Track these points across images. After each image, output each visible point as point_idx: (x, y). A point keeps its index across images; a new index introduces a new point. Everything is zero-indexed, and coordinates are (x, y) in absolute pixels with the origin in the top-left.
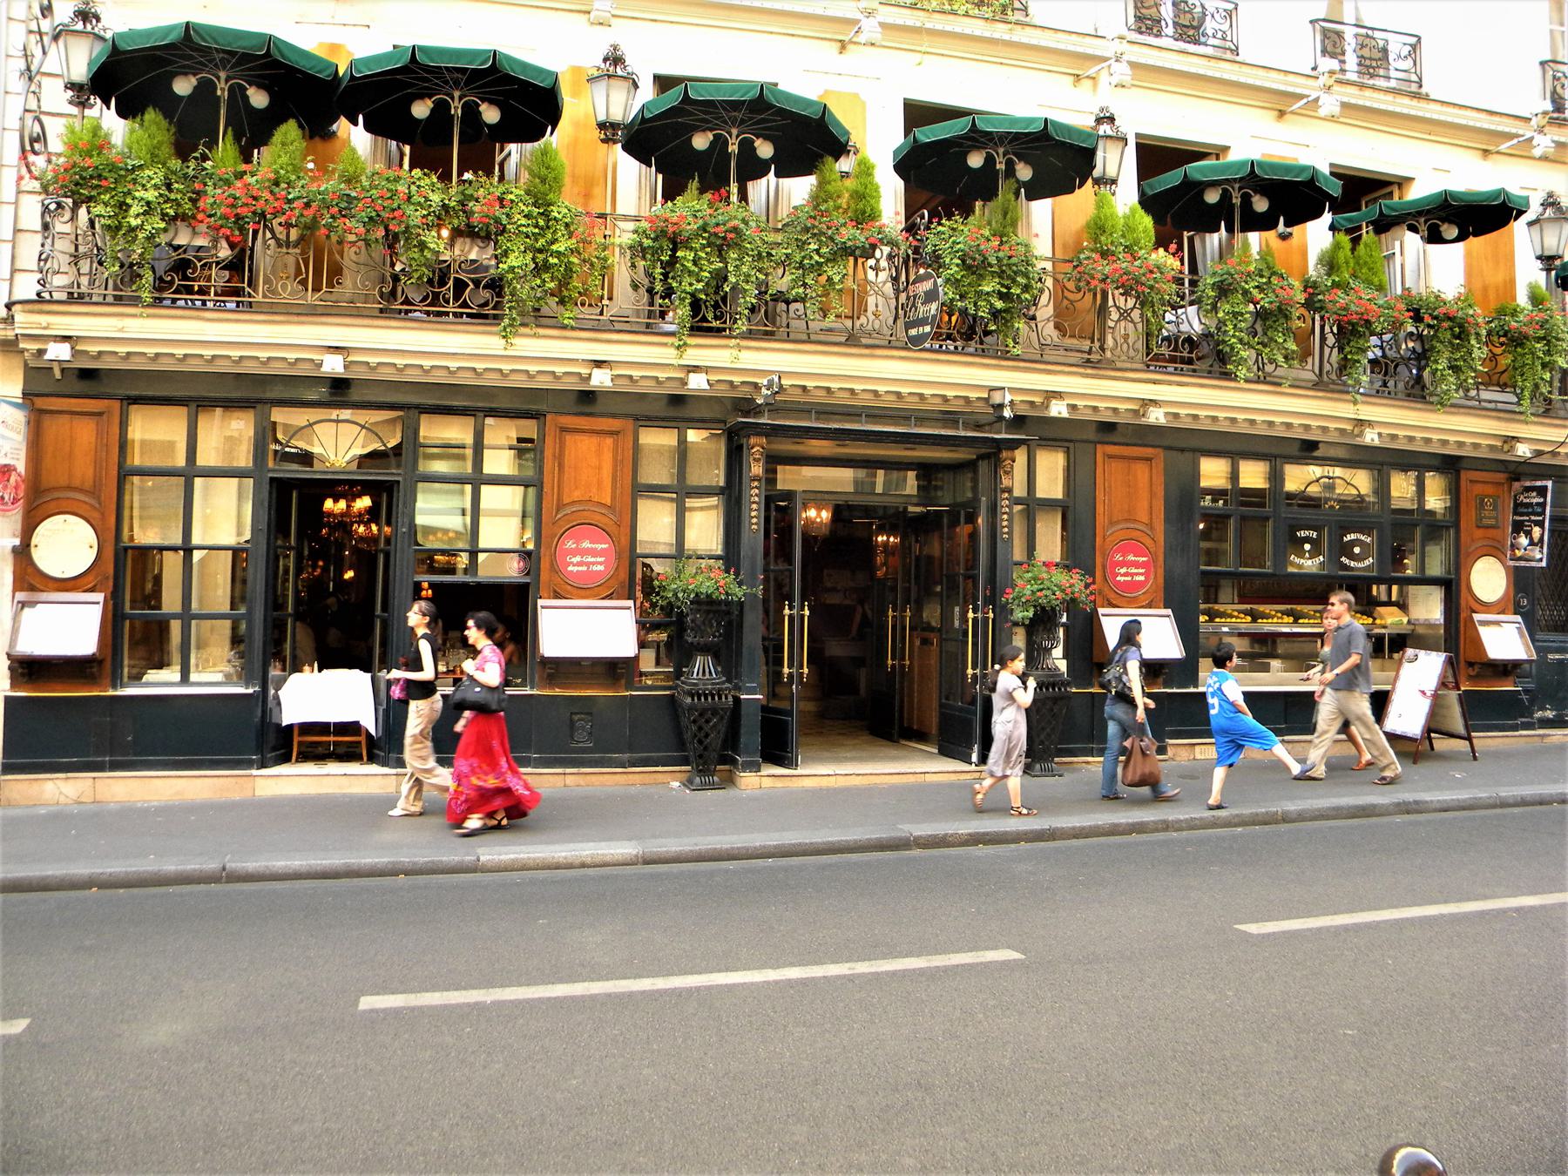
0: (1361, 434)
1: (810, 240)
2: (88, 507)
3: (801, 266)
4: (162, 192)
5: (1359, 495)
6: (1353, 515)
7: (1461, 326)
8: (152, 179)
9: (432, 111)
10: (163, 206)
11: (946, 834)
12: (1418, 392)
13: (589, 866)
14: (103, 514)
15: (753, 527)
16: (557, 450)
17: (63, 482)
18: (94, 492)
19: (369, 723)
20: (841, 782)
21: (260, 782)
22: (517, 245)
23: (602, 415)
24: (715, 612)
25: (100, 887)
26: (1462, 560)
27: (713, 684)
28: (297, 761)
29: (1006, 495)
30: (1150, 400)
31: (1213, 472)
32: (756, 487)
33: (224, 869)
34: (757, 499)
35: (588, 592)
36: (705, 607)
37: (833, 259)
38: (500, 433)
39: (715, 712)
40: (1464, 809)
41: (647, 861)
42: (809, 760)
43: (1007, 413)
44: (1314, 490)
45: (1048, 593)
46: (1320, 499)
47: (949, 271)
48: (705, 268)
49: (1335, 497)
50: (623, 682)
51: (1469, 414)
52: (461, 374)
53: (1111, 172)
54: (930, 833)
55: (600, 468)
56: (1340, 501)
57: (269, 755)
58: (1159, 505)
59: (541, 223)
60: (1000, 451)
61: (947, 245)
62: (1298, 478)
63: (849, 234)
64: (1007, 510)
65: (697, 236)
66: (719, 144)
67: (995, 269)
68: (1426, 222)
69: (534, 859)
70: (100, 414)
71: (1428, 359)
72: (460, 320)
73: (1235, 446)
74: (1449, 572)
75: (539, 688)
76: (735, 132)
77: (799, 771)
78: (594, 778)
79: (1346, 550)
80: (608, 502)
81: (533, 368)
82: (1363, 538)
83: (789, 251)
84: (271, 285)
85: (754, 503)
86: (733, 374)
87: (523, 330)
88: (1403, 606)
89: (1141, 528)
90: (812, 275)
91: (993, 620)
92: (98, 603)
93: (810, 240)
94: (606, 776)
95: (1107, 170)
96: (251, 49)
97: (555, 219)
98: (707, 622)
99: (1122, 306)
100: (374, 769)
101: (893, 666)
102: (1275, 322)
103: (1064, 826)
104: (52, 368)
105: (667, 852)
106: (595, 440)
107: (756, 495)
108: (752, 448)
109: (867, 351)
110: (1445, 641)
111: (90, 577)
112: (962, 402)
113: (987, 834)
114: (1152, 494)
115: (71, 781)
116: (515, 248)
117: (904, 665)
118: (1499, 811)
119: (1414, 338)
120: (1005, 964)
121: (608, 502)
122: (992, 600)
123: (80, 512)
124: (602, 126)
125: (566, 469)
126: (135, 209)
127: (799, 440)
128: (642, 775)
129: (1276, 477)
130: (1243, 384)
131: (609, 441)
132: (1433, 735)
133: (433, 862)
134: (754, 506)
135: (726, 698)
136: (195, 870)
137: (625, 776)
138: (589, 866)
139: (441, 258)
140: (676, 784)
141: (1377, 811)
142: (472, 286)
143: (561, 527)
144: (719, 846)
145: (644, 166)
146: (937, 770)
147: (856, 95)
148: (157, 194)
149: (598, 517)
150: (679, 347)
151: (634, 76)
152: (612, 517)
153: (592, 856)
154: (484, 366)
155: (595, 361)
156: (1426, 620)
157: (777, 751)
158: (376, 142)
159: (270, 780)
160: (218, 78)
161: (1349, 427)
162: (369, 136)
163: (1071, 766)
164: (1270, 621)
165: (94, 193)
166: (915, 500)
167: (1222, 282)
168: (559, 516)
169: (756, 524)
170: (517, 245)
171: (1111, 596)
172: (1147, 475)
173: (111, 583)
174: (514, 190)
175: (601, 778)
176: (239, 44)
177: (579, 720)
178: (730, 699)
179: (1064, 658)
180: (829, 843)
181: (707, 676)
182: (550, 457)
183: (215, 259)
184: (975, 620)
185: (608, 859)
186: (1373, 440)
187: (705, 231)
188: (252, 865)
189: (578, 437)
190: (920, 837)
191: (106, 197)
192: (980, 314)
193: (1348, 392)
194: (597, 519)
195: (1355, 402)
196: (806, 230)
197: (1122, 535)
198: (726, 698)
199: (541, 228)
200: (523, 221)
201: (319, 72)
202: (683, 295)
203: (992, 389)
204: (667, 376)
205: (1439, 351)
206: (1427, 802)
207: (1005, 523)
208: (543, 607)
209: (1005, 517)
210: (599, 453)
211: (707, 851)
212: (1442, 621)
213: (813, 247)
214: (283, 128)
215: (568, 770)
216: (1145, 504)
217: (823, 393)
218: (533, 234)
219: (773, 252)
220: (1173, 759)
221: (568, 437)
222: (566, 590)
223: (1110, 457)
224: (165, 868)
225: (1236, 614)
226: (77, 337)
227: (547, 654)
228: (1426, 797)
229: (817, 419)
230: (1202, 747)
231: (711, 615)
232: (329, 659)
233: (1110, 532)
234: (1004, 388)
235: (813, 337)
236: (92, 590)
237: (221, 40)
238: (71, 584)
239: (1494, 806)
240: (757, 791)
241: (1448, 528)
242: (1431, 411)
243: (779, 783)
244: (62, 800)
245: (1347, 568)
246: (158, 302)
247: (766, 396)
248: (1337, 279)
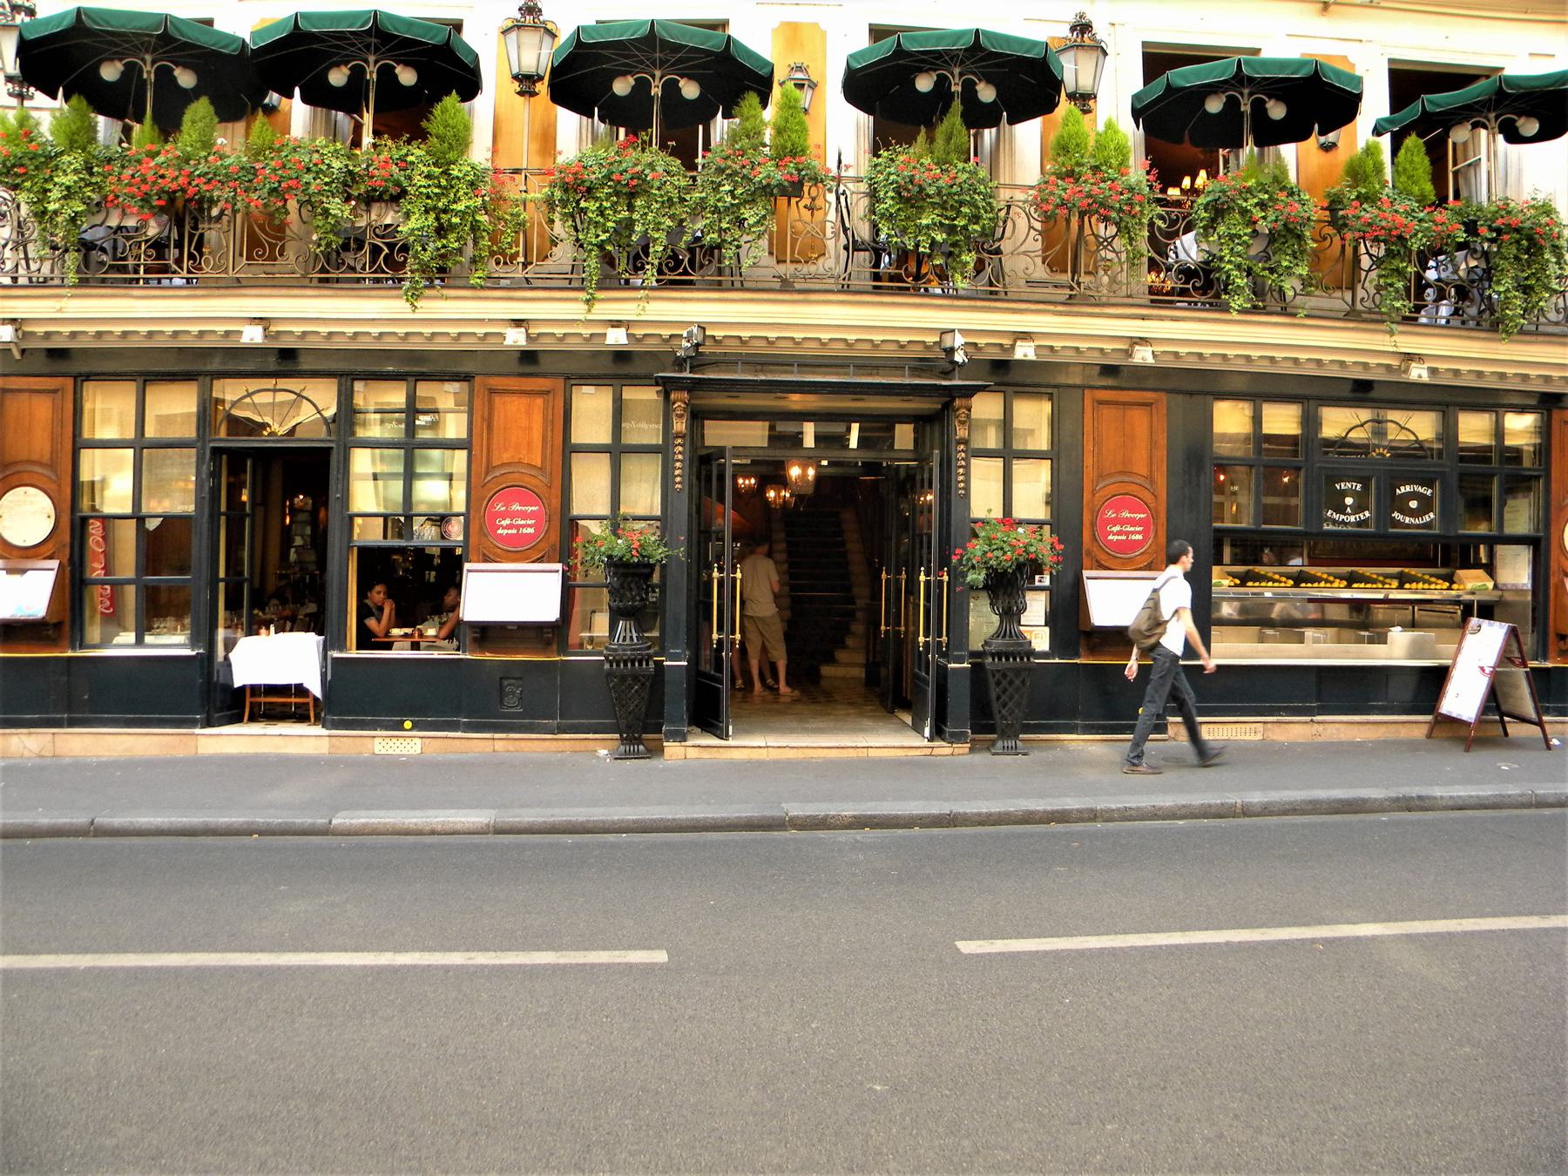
0: (1406, 371)
1: (725, 182)
2: (45, 479)
3: (716, 210)
4: (82, 176)
5: (1417, 441)
6: (1412, 460)
7: (1530, 239)
8: (72, 164)
9: (350, 77)
10: (85, 190)
11: (827, 815)
13: (439, 834)
14: (59, 485)
15: (677, 486)
16: (486, 413)
17: (24, 456)
18: (52, 465)
19: (316, 689)
20: (775, 755)
21: (202, 740)
22: (417, 209)
23: (544, 375)
24: (634, 575)
25: (261, 833)
26: (1553, 515)
27: (634, 650)
29: (962, 447)
30: (1140, 338)
32: (962, 451)
33: (92, 823)
34: (680, 457)
35: (519, 555)
36: (621, 570)
37: (751, 201)
38: (445, 396)
39: (636, 678)
40: (1486, 807)
41: (499, 831)
42: (742, 731)
44: (1358, 436)
45: (999, 553)
46: (1366, 446)
47: (883, 206)
48: (610, 217)
49: (1386, 443)
50: (555, 646)
51: (1549, 343)
52: (806, 345)
54: (808, 814)
55: (530, 429)
56: (1391, 449)
57: (217, 715)
58: (1161, 454)
59: (443, 182)
60: (953, 399)
61: (882, 178)
62: (1337, 422)
64: (963, 463)
65: (603, 185)
67: (936, 200)
68: (1497, 118)
69: (385, 824)
70: (55, 391)
71: (1490, 280)
72: (380, 285)
74: (1537, 530)
75: (472, 652)
76: (658, 73)
77: (731, 742)
78: (523, 743)
79: (1401, 504)
80: (539, 464)
82: (1421, 490)
83: (704, 195)
84: (195, 260)
85: (960, 467)
86: (659, 327)
87: (427, 292)
88: (1490, 569)
89: (1138, 481)
90: (727, 219)
91: (741, 580)
92: (52, 570)
93: (725, 182)
94: (457, 742)
95: (1081, 83)
96: (147, 29)
97: (458, 178)
98: (625, 585)
99: (1102, 234)
100: (318, 730)
101: (886, 631)
102: (1284, 243)
103: (968, 811)
104: (10, 350)
105: (519, 822)
106: (525, 400)
107: (680, 453)
108: (674, 404)
109: (801, 297)
110: (1534, 610)
111: (50, 545)
112: (894, 347)
113: (875, 817)
115: (33, 737)
116: (416, 210)
117: (899, 631)
119: (1478, 255)
121: (539, 464)
122: (944, 561)
123: (39, 484)
125: (495, 431)
126: (55, 194)
127: (783, 395)
128: (572, 742)
129: (1310, 422)
130: (1235, 316)
131: (539, 401)
132: (1506, 719)
133: (286, 823)
134: (678, 464)
135: (647, 664)
136: (65, 823)
137: (555, 743)
138: (439, 834)
139: (357, 225)
140: (603, 752)
142: (386, 251)
143: (490, 490)
144: (574, 819)
145: (585, 118)
146: (881, 745)
148: (75, 178)
149: (527, 479)
150: (588, 301)
151: (1103, 44)
152: (543, 479)
153: (443, 823)
154: (749, 334)
155: (513, 320)
156: (1513, 585)
157: (707, 717)
158: (314, 117)
162: (307, 108)
163: (1050, 744)
164: (1316, 585)
165: (18, 181)
166: (911, 456)
167: (1216, 200)
168: (488, 478)
169: (679, 483)
172: (1146, 424)
173: (67, 551)
174: (415, 151)
175: (530, 743)
176: (133, 25)
177: (509, 685)
178: (652, 665)
179: (1046, 625)
181: (628, 642)
182: (479, 419)
183: (144, 238)
185: (459, 827)
186: (1420, 376)
187: (610, 180)
188: (118, 821)
189: (507, 398)
190: (797, 817)
191: (28, 184)
192: (921, 249)
193: (1383, 322)
194: (527, 481)
195: (1391, 333)
196: (720, 171)
197: (1112, 489)
198: (647, 664)
199: (445, 188)
200: (424, 182)
201: (224, 47)
202: (590, 247)
203: (944, 332)
204: (908, 339)
205: (1502, 270)
206: (1435, 798)
207: (961, 478)
208: (469, 571)
209: (961, 471)
210: (529, 413)
211: (635, 822)
212: (1529, 586)
213: (727, 188)
215: (497, 736)
218: (436, 194)
219: (688, 197)
220: (1174, 739)
221: (497, 399)
222: (495, 554)
223: (1101, 403)
224: (39, 821)
225: (1277, 577)
226: (22, 319)
227: (1096, 624)
228: (1438, 792)
229: (911, 376)
230: (1211, 726)
231: (630, 579)
232: (289, 623)
233: (1101, 485)
234: (953, 331)
236: (50, 557)
237: (113, 23)
238: (31, 552)
239: (1529, 805)
240: (680, 762)
241: (1537, 478)
243: (706, 754)
244: (26, 753)
246: (83, 283)
247: (687, 349)
248: (1363, 191)
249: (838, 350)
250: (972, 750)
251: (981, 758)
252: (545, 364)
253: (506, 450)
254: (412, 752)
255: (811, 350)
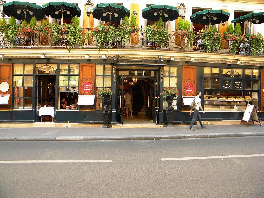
3: (121, 35)
6: (238, 78)
7: (258, 40)
12: (251, 54)
17: (4, 77)
18: (9, 78)
22: (70, 35)
26: (261, 87)
28: (42, 121)
31: (207, 71)
38: (75, 67)
43: (161, 60)
44: (229, 73)
46: (230, 75)
53: (183, 14)
56: (234, 76)
58: (196, 77)
63: (129, 29)
66: (108, 15)
68: (252, 20)
70: (9, 66)
73: (212, 65)
74: (259, 89)
75: (79, 110)
77: (123, 125)
81: (134, 56)
100: (54, 123)
106: (88, 67)
109: (135, 50)
114: (194, 75)
118: (258, 137)
120: (109, 163)
122: (159, 94)
124: (87, 13)
126: (9, 33)
129: (221, 71)
130: (208, 53)
131: (91, 67)
140: (101, 127)
141: (230, 136)
147: (137, 4)
150: (99, 51)
157: (119, 120)
159: (36, 124)
160: (24, 10)
161: (235, 61)
170: (70, 35)
171: (185, 94)
173: (11, 93)
180: (117, 138)
184: (156, 98)
188: (20, 138)
189: (86, 67)
195: (234, 56)
197: (187, 82)
200: (71, 31)
201: (38, 8)
203: (159, 56)
206: (241, 134)
209: (162, 79)
214: (33, 18)
216: (193, 77)
217: (197, 60)
221: (84, 67)
223: (185, 68)
228: (242, 133)
235: (126, 48)
241: (259, 80)
242: (252, 57)
243: (119, 127)
245: (235, 88)
246: (14, 48)
247: (116, 59)
249: (141, 59)
250: (164, 126)
251: (165, 128)
252: (92, 61)
253: (85, 76)
254: (69, 127)
255: (136, 59)
